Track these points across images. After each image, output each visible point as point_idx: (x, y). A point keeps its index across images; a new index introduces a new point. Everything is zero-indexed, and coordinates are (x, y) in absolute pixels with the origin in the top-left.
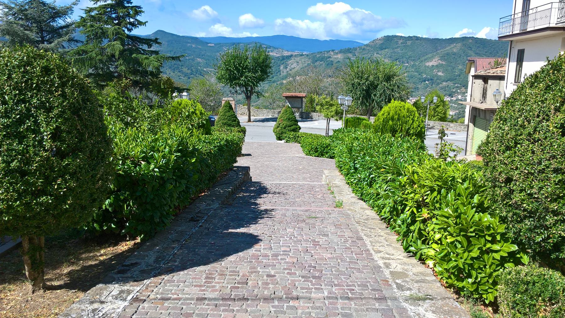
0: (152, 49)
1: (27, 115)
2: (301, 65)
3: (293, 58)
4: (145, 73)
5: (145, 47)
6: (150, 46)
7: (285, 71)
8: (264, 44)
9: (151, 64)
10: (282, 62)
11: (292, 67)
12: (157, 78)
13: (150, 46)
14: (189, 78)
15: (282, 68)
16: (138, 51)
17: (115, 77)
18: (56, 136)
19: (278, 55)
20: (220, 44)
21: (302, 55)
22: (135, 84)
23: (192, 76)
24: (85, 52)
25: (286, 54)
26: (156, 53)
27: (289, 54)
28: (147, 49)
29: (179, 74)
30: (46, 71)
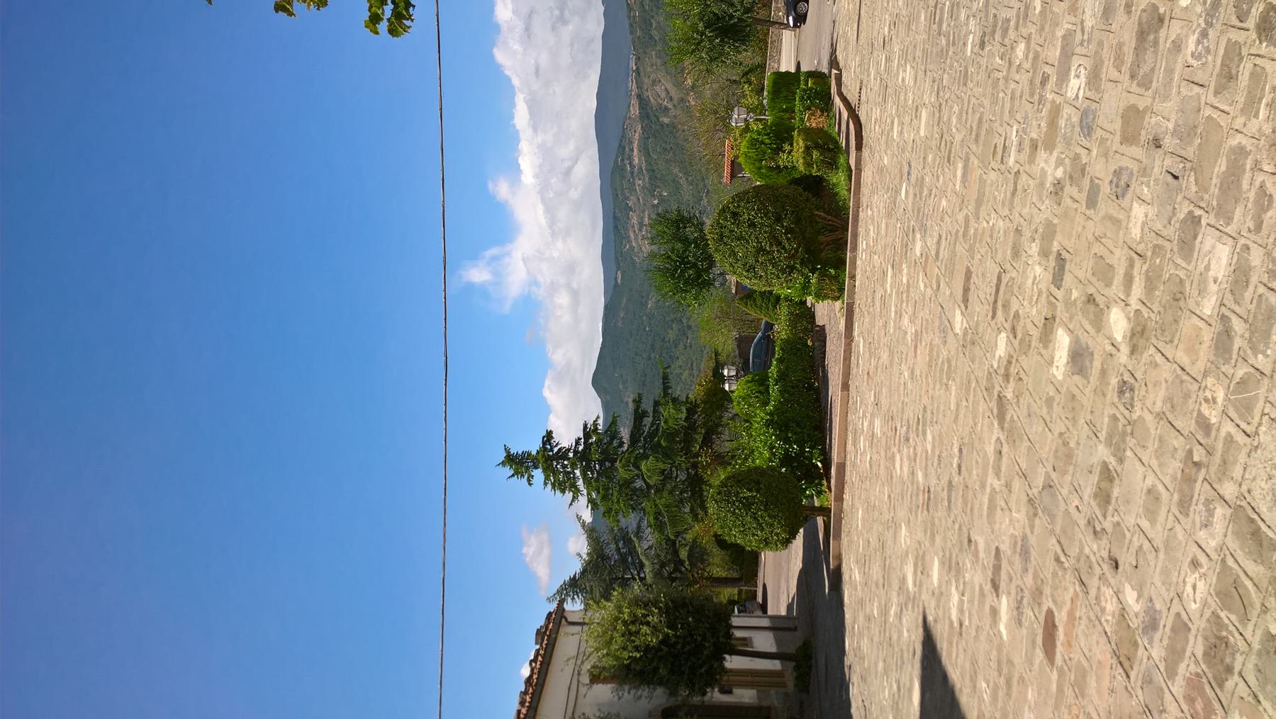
0: (650, 410)
1: (741, 502)
2: (660, 75)
3: (646, 94)
4: (691, 427)
5: (648, 421)
6: (645, 414)
7: (673, 112)
8: (616, 161)
9: (673, 416)
10: (654, 119)
11: (663, 95)
12: (697, 406)
13: (645, 414)
14: (689, 327)
15: (666, 120)
16: (652, 435)
17: (696, 473)
18: (750, 490)
19: (639, 129)
20: (617, 258)
21: (638, 71)
22: (707, 441)
23: (684, 321)
24: (658, 514)
25: (635, 110)
26: (656, 404)
27: (635, 102)
28: (650, 419)
29: (681, 346)
30: (719, 493)
